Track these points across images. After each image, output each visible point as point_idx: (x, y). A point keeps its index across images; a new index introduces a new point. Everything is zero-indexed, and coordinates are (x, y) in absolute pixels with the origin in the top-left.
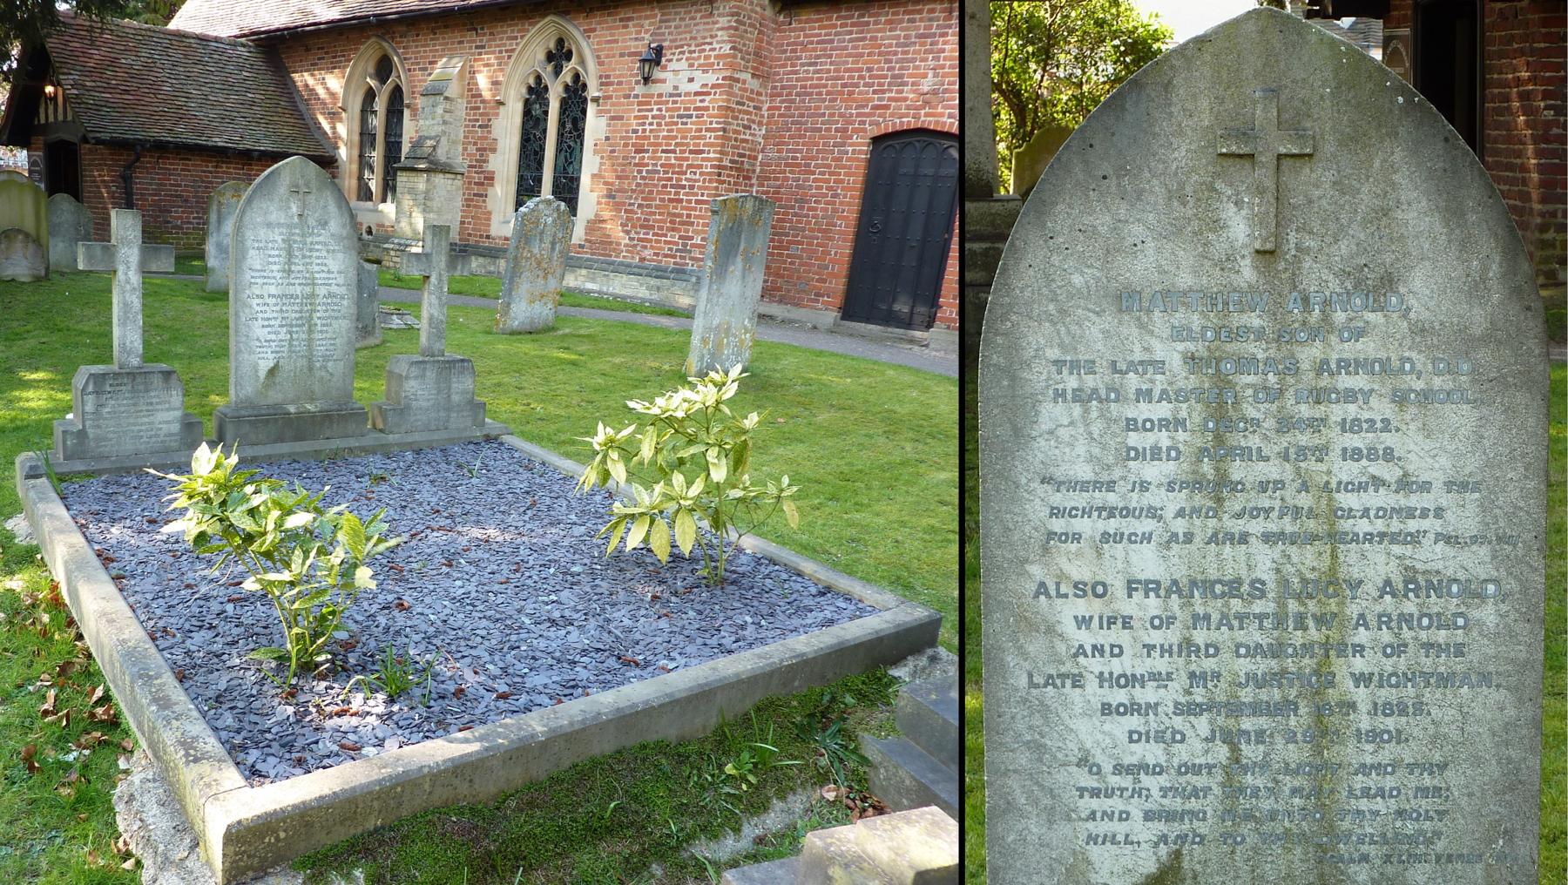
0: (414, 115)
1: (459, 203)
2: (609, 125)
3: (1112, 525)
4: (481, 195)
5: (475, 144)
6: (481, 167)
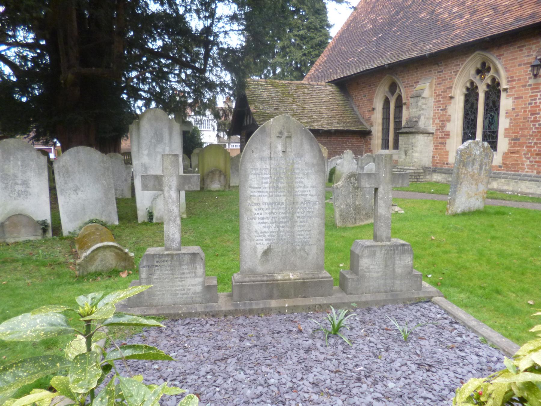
0: (408, 108)
1: (431, 148)
2: (514, 102)
3: (260, 194)
4: (443, 143)
5: (439, 118)
6: (442, 129)
